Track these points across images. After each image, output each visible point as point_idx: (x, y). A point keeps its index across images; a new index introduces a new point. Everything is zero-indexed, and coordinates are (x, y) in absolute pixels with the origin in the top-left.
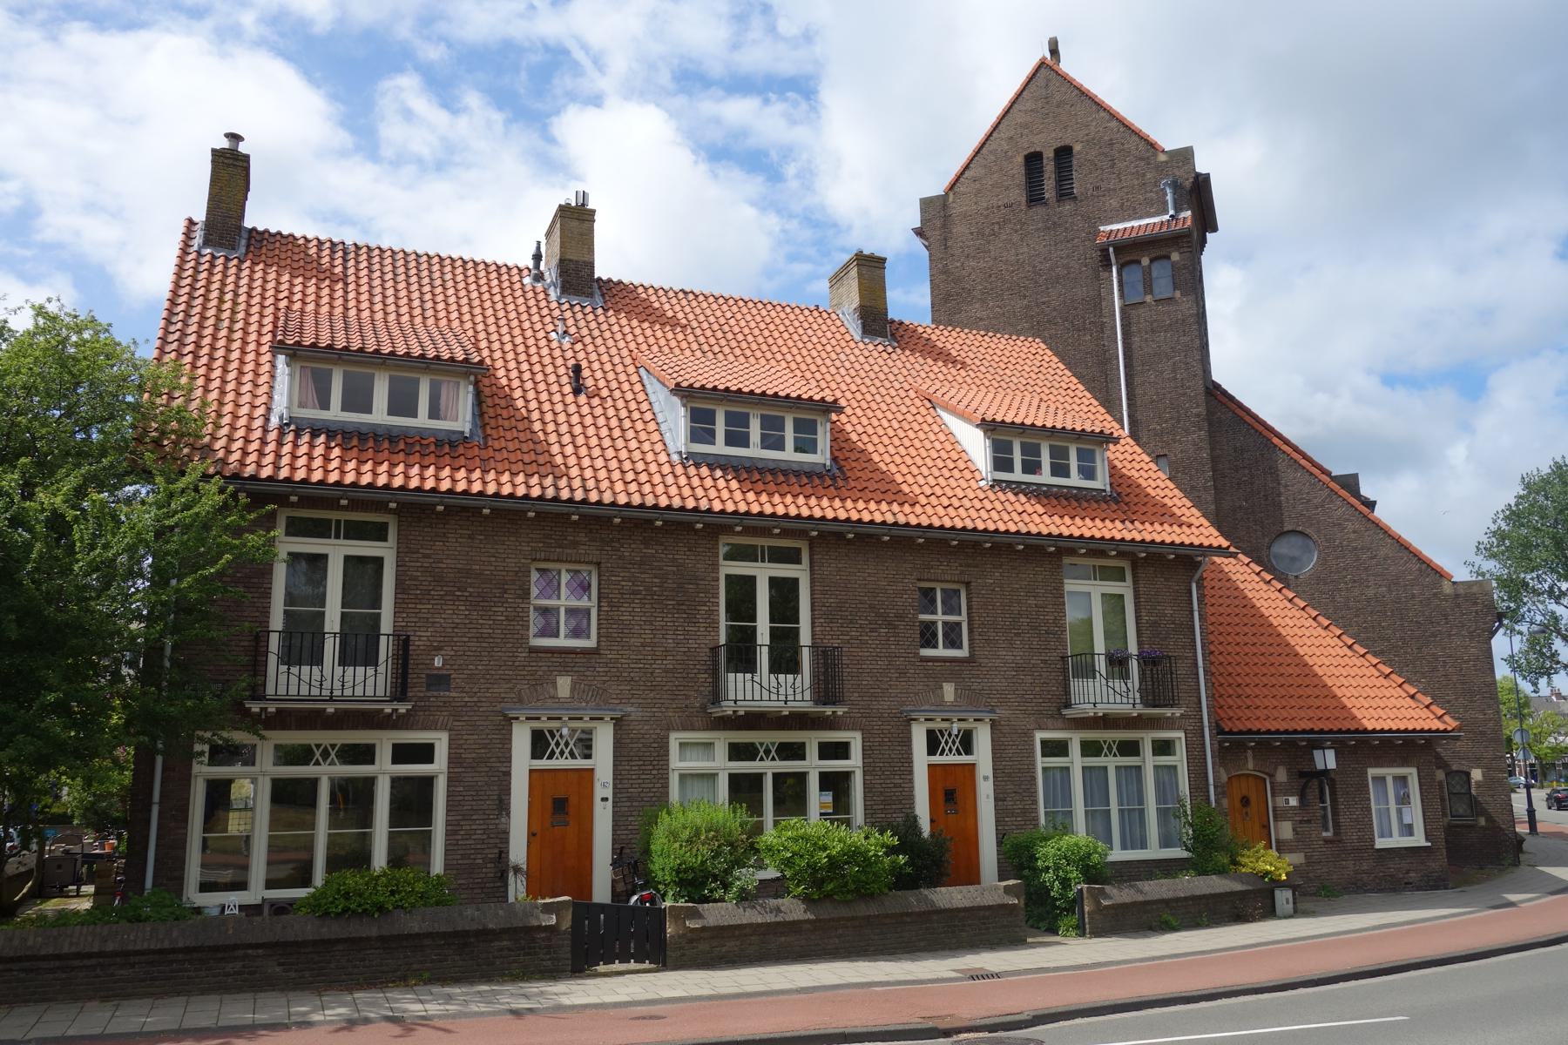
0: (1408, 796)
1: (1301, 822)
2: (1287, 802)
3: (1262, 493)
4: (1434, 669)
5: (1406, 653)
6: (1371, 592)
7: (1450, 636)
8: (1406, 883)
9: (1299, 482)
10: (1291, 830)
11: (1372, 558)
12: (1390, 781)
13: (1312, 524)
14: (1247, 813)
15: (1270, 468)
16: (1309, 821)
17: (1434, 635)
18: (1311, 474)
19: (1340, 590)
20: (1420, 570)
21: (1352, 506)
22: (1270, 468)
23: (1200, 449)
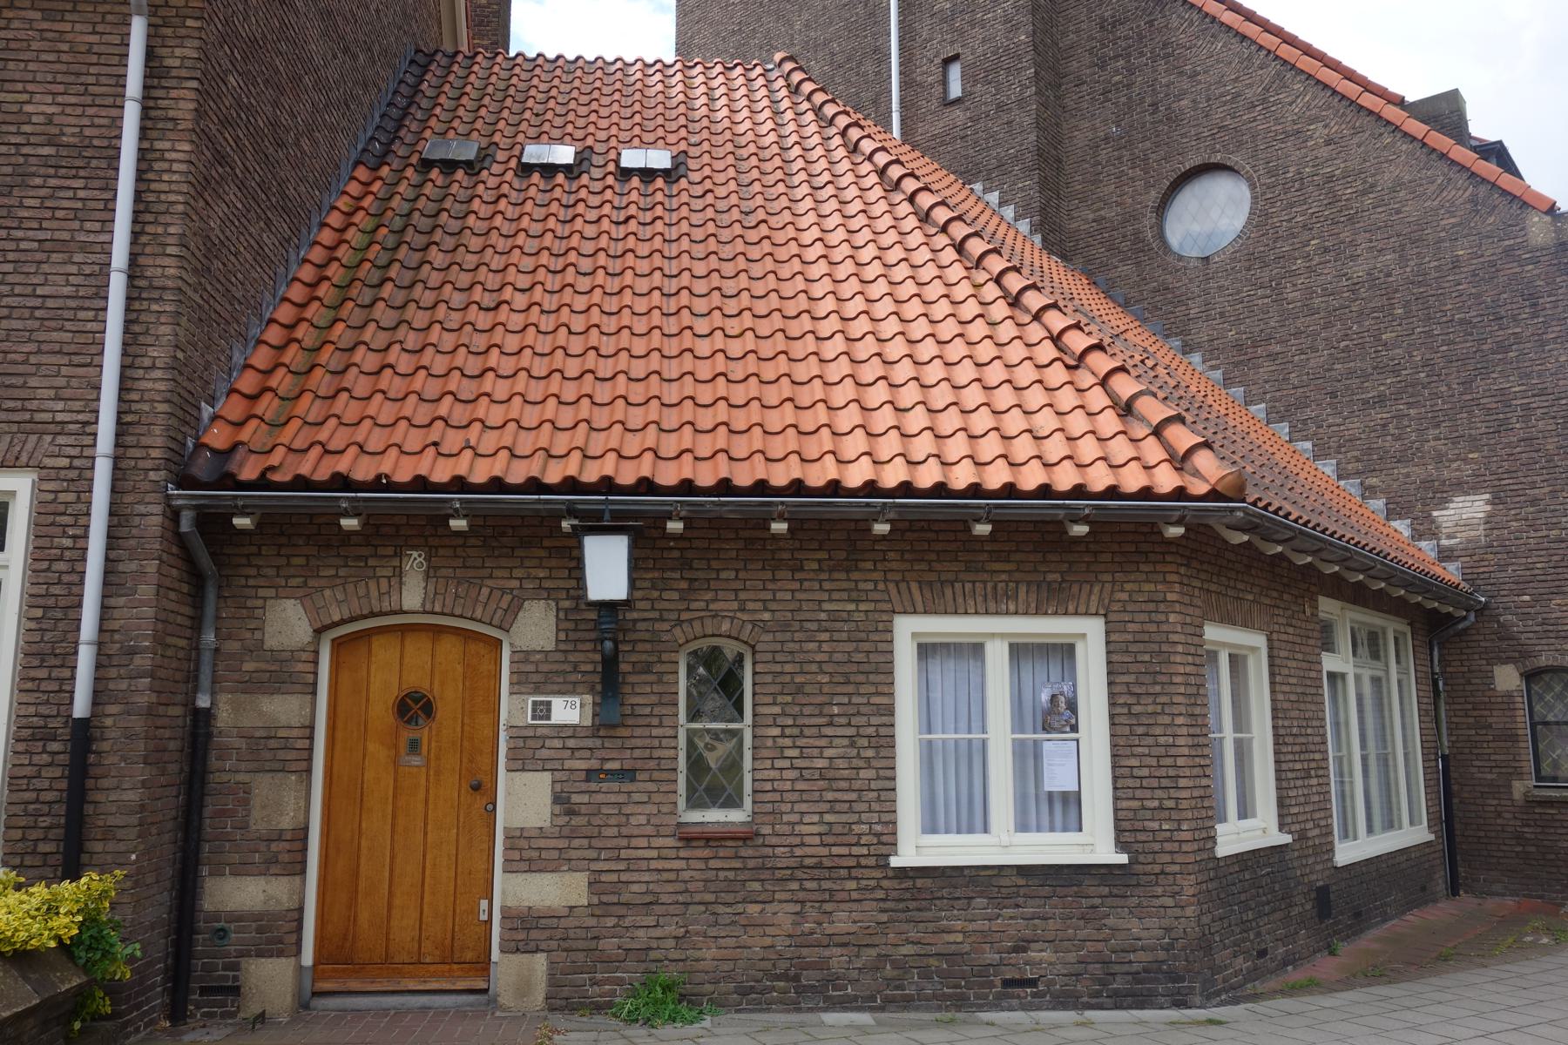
0: (1072, 706)
1: (590, 774)
2: (543, 710)
3: (1148, 100)
4: (1502, 427)
5: (1437, 395)
6: (1359, 270)
7: (1543, 343)
8: (1008, 983)
9: (1218, 61)
10: (547, 799)
11: (1364, 193)
12: (997, 657)
13: (1241, 144)
14: (414, 746)
15: (1165, 45)
16: (627, 774)
17: (1502, 348)
18: (1244, 37)
19: (1294, 274)
20: (1473, 200)
21: (1326, 86)
22: (1165, 45)
23: (1015, 28)
